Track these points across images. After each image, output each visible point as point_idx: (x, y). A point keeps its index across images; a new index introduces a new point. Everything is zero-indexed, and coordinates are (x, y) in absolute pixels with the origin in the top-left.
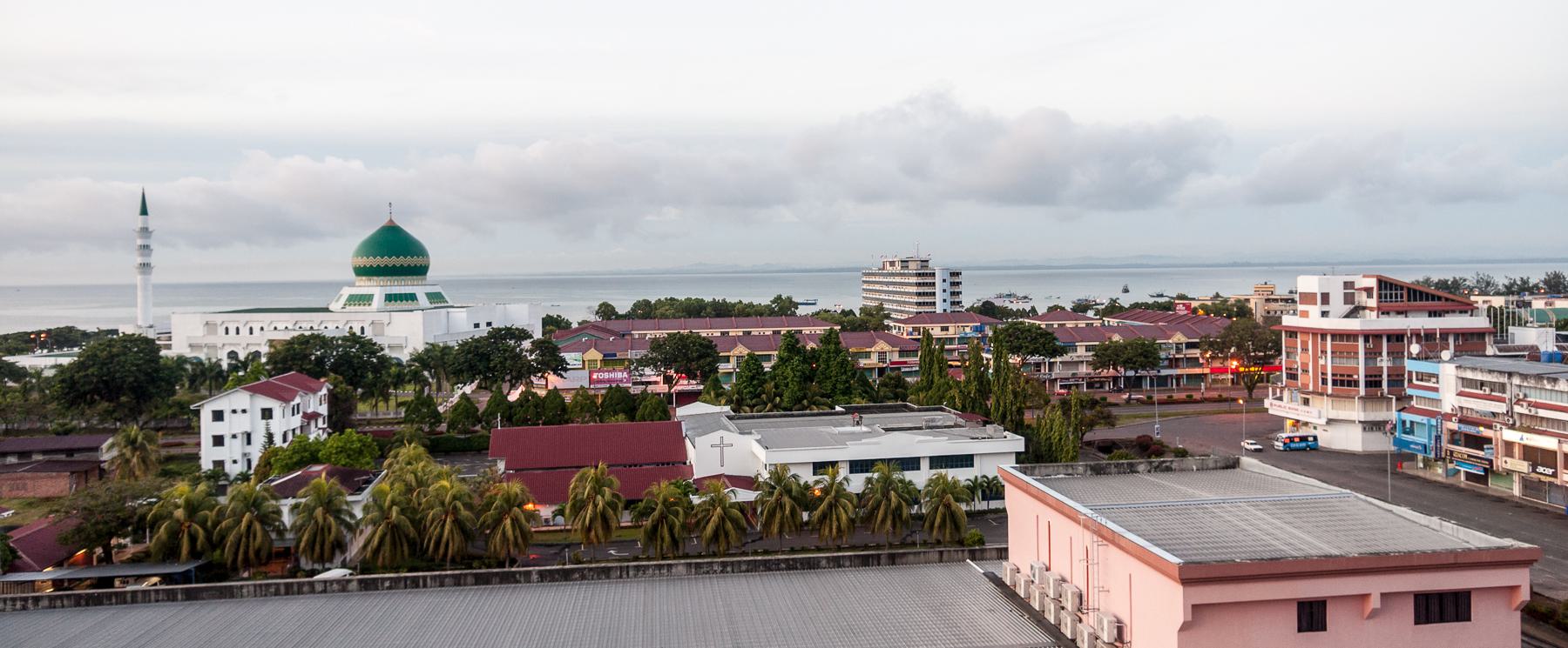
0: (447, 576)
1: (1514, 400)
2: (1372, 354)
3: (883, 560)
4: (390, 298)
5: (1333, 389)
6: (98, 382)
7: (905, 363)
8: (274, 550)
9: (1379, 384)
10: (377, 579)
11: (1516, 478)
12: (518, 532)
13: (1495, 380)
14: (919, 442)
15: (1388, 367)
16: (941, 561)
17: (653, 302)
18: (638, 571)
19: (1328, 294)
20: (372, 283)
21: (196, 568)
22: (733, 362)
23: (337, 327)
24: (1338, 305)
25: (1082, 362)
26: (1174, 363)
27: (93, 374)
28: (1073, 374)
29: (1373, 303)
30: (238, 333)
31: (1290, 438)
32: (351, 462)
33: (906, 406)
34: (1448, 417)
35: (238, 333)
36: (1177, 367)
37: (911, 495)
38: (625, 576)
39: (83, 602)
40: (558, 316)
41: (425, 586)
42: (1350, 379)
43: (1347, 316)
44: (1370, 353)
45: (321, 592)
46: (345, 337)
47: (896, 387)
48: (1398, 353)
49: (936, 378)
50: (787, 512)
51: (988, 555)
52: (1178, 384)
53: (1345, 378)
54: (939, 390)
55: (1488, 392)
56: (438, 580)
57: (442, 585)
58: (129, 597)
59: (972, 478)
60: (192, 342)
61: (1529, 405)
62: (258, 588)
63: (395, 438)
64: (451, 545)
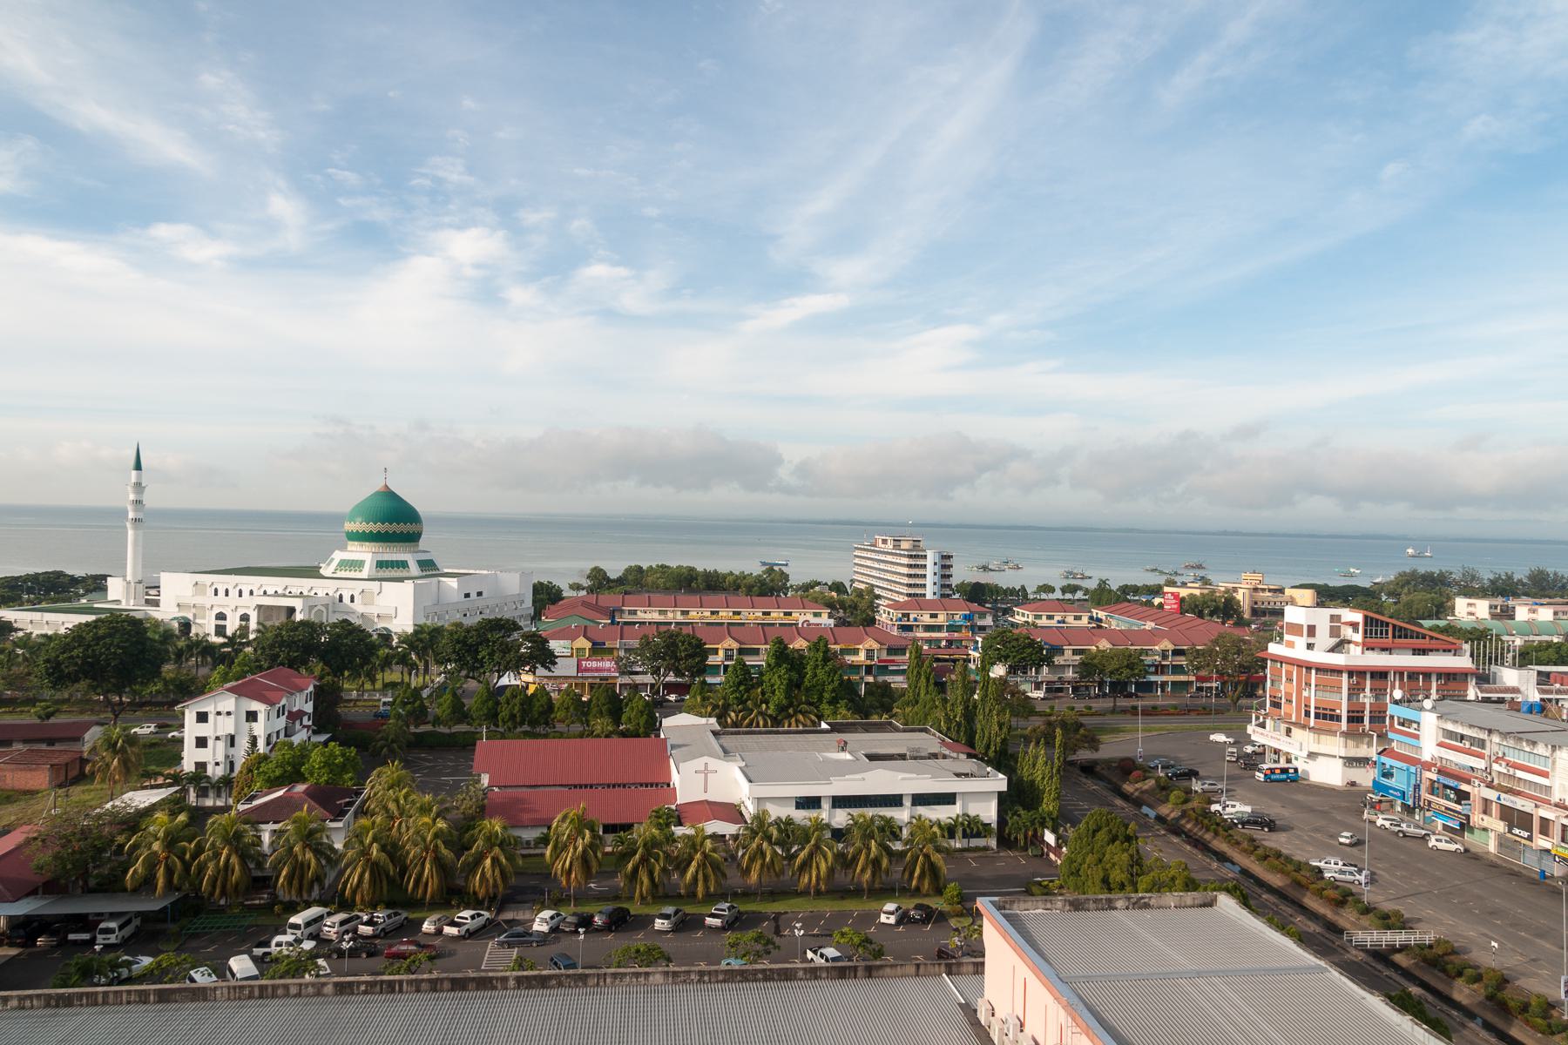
0: (423, 980)
1: (1493, 758)
2: (1355, 691)
3: (860, 973)
4: (381, 565)
5: (1315, 722)
6: (82, 664)
7: (893, 661)
8: (262, 834)
9: (1360, 720)
10: (353, 982)
11: (1492, 835)
12: (497, 872)
14: (903, 779)
15: (1371, 704)
17: (645, 568)
18: (615, 978)
22: (721, 653)
23: (327, 594)
24: (1324, 639)
25: (1069, 665)
26: (1160, 669)
27: (78, 657)
28: (1060, 678)
29: (1358, 637)
30: (227, 595)
31: (1270, 769)
32: (335, 777)
33: (890, 724)
34: (1427, 766)
35: (227, 595)
36: (1163, 673)
37: (890, 830)
38: (602, 983)
39: (53, 1003)
40: (548, 582)
41: (401, 991)
42: (1333, 713)
43: (1332, 650)
44: (1354, 689)
45: (295, 996)
46: (334, 623)
47: (883, 695)
48: (1380, 690)
49: (922, 695)
50: (768, 860)
51: (964, 969)
52: (1163, 691)
53: (1328, 712)
54: (925, 707)
55: (1468, 746)
56: (414, 984)
57: (418, 991)
58: (100, 999)
59: (954, 816)
61: (1507, 765)
62: (232, 991)
63: (380, 736)
64: (430, 884)
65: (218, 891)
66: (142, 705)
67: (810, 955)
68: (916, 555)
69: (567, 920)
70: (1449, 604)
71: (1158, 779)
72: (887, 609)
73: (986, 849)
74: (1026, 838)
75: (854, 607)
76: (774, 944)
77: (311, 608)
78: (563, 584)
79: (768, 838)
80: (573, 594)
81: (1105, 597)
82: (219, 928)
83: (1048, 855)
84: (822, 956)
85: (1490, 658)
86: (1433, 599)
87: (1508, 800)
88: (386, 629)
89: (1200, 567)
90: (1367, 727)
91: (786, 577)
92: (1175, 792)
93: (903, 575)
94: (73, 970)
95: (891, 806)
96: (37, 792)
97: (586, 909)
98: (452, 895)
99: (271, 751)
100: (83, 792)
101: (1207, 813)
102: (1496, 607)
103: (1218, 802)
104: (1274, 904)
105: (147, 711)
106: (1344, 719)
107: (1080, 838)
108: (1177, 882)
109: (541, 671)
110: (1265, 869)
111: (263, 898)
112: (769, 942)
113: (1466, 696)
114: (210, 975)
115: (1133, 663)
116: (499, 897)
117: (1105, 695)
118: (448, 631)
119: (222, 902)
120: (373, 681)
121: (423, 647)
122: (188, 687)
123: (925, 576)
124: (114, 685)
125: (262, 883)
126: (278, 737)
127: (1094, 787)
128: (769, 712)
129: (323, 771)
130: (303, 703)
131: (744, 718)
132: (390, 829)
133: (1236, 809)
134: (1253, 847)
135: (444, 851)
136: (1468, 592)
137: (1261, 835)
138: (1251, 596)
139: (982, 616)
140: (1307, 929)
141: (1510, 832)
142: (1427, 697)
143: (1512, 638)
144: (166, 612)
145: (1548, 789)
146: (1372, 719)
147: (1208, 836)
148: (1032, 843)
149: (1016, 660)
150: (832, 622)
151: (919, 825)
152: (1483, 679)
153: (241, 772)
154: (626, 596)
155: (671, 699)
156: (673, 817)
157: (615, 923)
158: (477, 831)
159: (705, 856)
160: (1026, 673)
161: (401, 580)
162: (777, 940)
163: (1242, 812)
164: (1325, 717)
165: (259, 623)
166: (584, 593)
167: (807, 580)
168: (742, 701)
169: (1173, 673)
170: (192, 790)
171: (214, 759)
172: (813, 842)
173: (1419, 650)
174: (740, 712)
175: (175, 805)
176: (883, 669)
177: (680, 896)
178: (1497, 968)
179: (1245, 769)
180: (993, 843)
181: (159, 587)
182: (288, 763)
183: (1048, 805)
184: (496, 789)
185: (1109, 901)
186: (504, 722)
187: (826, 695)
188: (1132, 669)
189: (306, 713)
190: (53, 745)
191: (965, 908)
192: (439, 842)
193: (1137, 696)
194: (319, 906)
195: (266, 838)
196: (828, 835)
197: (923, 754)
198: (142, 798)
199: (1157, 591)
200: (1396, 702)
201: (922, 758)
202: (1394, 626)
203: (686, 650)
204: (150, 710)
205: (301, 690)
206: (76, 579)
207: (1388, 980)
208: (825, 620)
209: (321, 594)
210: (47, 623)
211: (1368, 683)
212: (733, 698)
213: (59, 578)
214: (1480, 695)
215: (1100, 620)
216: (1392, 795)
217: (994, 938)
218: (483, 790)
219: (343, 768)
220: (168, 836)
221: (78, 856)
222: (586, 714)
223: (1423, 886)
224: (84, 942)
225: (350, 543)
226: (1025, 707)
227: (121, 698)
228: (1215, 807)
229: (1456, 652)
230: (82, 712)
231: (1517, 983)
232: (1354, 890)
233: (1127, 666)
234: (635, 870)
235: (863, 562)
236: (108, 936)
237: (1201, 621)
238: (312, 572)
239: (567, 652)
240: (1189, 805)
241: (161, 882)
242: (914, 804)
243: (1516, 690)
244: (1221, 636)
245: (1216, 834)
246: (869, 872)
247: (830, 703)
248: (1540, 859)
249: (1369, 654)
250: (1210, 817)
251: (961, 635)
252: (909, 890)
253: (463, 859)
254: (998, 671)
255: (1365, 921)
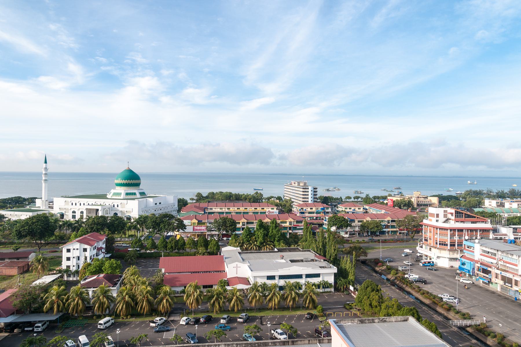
1: (499, 259)
2: (452, 236)
3: (290, 343)
4: (127, 194)
7: (298, 225)
8: (89, 292)
9: (454, 245)
11: (499, 285)
13: (493, 252)
14: (302, 269)
15: (458, 240)
16: (309, 344)
17: (215, 193)
19: (438, 214)
20: (121, 189)
21: (59, 317)
22: (241, 224)
24: (442, 219)
26: (387, 227)
27: (27, 229)
28: (354, 230)
30: (76, 205)
31: (425, 262)
34: (477, 262)
35: (76, 205)
36: (388, 228)
37: (298, 286)
42: (445, 243)
43: (444, 222)
44: (452, 235)
47: (295, 238)
48: (461, 235)
49: (308, 239)
51: (325, 341)
52: (388, 234)
53: (443, 243)
55: (490, 255)
59: (320, 281)
60: (60, 207)
63: (128, 255)
64: (145, 308)
65: (75, 312)
66: (48, 244)
67: (272, 332)
68: (305, 188)
69: (191, 320)
70: (483, 201)
71: (387, 266)
72: (296, 207)
73: (330, 292)
74: (344, 288)
75: (285, 205)
76: (261, 329)
77: (104, 209)
78: (187, 199)
79: (258, 291)
80: (191, 201)
81: (368, 200)
82: (75, 325)
83: (351, 294)
84: (277, 332)
85: (497, 222)
86: (477, 200)
87: (504, 274)
88: (129, 216)
89: (399, 188)
90: (457, 248)
91: (261, 195)
92: (393, 271)
93: (301, 191)
94: (27, 342)
95: (299, 278)
96: (14, 276)
97: (198, 316)
98: (154, 311)
99: (92, 261)
100: (29, 276)
101: (404, 278)
102: (498, 203)
103: (407, 274)
104: (427, 310)
105: (50, 246)
106: (449, 245)
107: (362, 290)
108: (394, 306)
109: (181, 231)
110: (423, 298)
111: (90, 313)
112: (259, 328)
113: (489, 237)
114: (72, 343)
115: (378, 225)
116: (169, 312)
117: (369, 236)
118: (150, 217)
119: (76, 315)
120: (125, 235)
121: (141, 223)
122: (64, 238)
123: (308, 195)
124: (39, 238)
125: (89, 308)
126: (94, 257)
127: (366, 269)
128: (257, 244)
129: (109, 269)
130: (102, 244)
131: (249, 247)
132: (132, 290)
133: (413, 276)
134: (419, 290)
135: (150, 297)
136: (490, 196)
137: (421, 285)
138: (417, 200)
139: (327, 208)
140: (438, 320)
141: (505, 284)
142: (476, 238)
143: (504, 214)
144: (56, 211)
145: (517, 270)
146: (458, 245)
147: (404, 286)
148: (346, 290)
149: (339, 225)
150: (278, 211)
151: (307, 284)
152: (495, 231)
153: (82, 269)
154: (209, 215)
155: (224, 239)
156: (226, 283)
157: (207, 321)
158: (161, 290)
159: (237, 297)
160: (342, 229)
161: (134, 199)
162: (262, 327)
163: (416, 278)
164: (442, 244)
165: (87, 216)
166: (195, 201)
167: (269, 196)
168: (248, 241)
169: (391, 228)
170: (65, 275)
171: (73, 264)
172: (272, 292)
173: (473, 222)
174: (248, 244)
175: (59, 282)
176: (295, 228)
177: (229, 311)
178: (501, 333)
179: (416, 262)
180: (332, 290)
181: (53, 202)
182: (98, 267)
183: (351, 277)
184: (167, 274)
185: (373, 320)
186: (169, 249)
187: (276, 239)
188: (378, 228)
189: (103, 248)
190: (19, 260)
191: (324, 314)
192: (148, 294)
193: (379, 236)
194: (108, 317)
195: (91, 293)
196: (278, 289)
197: (309, 260)
198: (47, 279)
199: (385, 198)
200: (466, 240)
201: (309, 261)
202: (465, 214)
203: (229, 224)
204: (51, 246)
205: (101, 240)
206: (25, 199)
207: (465, 338)
208: (275, 211)
209: (107, 204)
210: (16, 215)
211: (457, 233)
212: (246, 240)
213: (19, 199)
214: (494, 237)
215: (366, 209)
216: (465, 271)
217: (334, 332)
218: (162, 274)
219: (116, 268)
220: (58, 294)
221: (28, 301)
222: (197, 246)
223: (476, 303)
224: (30, 331)
225: (116, 187)
226: (343, 241)
227: (41, 242)
228: (406, 276)
229: (486, 222)
230: (28, 247)
231: (508, 338)
232: (453, 305)
233: (376, 227)
234: (214, 302)
235: (287, 190)
236: (38, 329)
237: (400, 210)
238: (104, 197)
239: (190, 224)
240: (398, 275)
241: (55, 310)
242: (306, 277)
243: (506, 235)
244: (407, 216)
245: (407, 285)
246: (292, 302)
247: (277, 241)
248: (515, 294)
249: (457, 223)
250: (405, 279)
251: (320, 215)
252: (305, 307)
253: (156, 300)
254: (333, 229)
255: (457, 316)
